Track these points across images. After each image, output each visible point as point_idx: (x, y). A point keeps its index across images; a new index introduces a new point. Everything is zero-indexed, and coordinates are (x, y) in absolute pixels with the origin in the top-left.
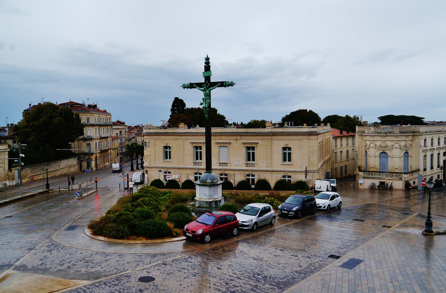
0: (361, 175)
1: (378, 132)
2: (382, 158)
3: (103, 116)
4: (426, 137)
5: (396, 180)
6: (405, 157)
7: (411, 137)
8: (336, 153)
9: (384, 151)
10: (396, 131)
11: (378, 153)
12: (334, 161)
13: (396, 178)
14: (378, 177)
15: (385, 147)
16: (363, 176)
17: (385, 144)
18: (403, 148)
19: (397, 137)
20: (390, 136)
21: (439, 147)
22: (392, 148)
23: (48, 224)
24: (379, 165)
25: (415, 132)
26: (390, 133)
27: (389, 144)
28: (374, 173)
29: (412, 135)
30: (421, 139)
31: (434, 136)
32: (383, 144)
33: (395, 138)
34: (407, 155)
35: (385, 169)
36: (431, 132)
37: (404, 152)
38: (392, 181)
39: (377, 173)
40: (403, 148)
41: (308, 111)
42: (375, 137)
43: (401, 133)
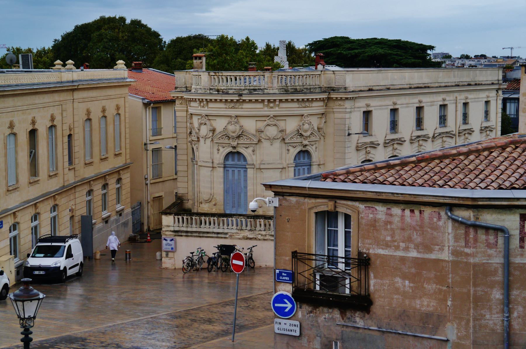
0: (168, 226)
1: (218, 91)
2: (230, 170)
4: (420, 102)
5: (264, 240)
6: (301, 168)
7: (321, 104)
8: (157, 152)
9: (234, 148)
10: (270, 85)
11: (219, 158)
12: (150, 176)
13: (263, 233)
14: (216, 230)
15: (239, 137)
16: (172, 229)
17: (238, 127)
18: (292, 138)
19: (272, 105)
20: (250, 101)
21: (419, 133)
22: (259, 141)
23: (114, 310)
24: (222, 193)
25: (333, 89)
26: (252, 91)
27: (250, 125)
28: (203, 218)
29: (323, 100)
30: (350, 112)
31: (399, 102)
32: (231, 128)
33: (266, 109)
34: (306, 160)
35: (239, 206)
36: (458, 86)
37: (294, 151)
38: (254, 243)
39: (212, 219)
40: (292, 138)
41: (128, 21)
42: (211, 105)
43: (286, 91)
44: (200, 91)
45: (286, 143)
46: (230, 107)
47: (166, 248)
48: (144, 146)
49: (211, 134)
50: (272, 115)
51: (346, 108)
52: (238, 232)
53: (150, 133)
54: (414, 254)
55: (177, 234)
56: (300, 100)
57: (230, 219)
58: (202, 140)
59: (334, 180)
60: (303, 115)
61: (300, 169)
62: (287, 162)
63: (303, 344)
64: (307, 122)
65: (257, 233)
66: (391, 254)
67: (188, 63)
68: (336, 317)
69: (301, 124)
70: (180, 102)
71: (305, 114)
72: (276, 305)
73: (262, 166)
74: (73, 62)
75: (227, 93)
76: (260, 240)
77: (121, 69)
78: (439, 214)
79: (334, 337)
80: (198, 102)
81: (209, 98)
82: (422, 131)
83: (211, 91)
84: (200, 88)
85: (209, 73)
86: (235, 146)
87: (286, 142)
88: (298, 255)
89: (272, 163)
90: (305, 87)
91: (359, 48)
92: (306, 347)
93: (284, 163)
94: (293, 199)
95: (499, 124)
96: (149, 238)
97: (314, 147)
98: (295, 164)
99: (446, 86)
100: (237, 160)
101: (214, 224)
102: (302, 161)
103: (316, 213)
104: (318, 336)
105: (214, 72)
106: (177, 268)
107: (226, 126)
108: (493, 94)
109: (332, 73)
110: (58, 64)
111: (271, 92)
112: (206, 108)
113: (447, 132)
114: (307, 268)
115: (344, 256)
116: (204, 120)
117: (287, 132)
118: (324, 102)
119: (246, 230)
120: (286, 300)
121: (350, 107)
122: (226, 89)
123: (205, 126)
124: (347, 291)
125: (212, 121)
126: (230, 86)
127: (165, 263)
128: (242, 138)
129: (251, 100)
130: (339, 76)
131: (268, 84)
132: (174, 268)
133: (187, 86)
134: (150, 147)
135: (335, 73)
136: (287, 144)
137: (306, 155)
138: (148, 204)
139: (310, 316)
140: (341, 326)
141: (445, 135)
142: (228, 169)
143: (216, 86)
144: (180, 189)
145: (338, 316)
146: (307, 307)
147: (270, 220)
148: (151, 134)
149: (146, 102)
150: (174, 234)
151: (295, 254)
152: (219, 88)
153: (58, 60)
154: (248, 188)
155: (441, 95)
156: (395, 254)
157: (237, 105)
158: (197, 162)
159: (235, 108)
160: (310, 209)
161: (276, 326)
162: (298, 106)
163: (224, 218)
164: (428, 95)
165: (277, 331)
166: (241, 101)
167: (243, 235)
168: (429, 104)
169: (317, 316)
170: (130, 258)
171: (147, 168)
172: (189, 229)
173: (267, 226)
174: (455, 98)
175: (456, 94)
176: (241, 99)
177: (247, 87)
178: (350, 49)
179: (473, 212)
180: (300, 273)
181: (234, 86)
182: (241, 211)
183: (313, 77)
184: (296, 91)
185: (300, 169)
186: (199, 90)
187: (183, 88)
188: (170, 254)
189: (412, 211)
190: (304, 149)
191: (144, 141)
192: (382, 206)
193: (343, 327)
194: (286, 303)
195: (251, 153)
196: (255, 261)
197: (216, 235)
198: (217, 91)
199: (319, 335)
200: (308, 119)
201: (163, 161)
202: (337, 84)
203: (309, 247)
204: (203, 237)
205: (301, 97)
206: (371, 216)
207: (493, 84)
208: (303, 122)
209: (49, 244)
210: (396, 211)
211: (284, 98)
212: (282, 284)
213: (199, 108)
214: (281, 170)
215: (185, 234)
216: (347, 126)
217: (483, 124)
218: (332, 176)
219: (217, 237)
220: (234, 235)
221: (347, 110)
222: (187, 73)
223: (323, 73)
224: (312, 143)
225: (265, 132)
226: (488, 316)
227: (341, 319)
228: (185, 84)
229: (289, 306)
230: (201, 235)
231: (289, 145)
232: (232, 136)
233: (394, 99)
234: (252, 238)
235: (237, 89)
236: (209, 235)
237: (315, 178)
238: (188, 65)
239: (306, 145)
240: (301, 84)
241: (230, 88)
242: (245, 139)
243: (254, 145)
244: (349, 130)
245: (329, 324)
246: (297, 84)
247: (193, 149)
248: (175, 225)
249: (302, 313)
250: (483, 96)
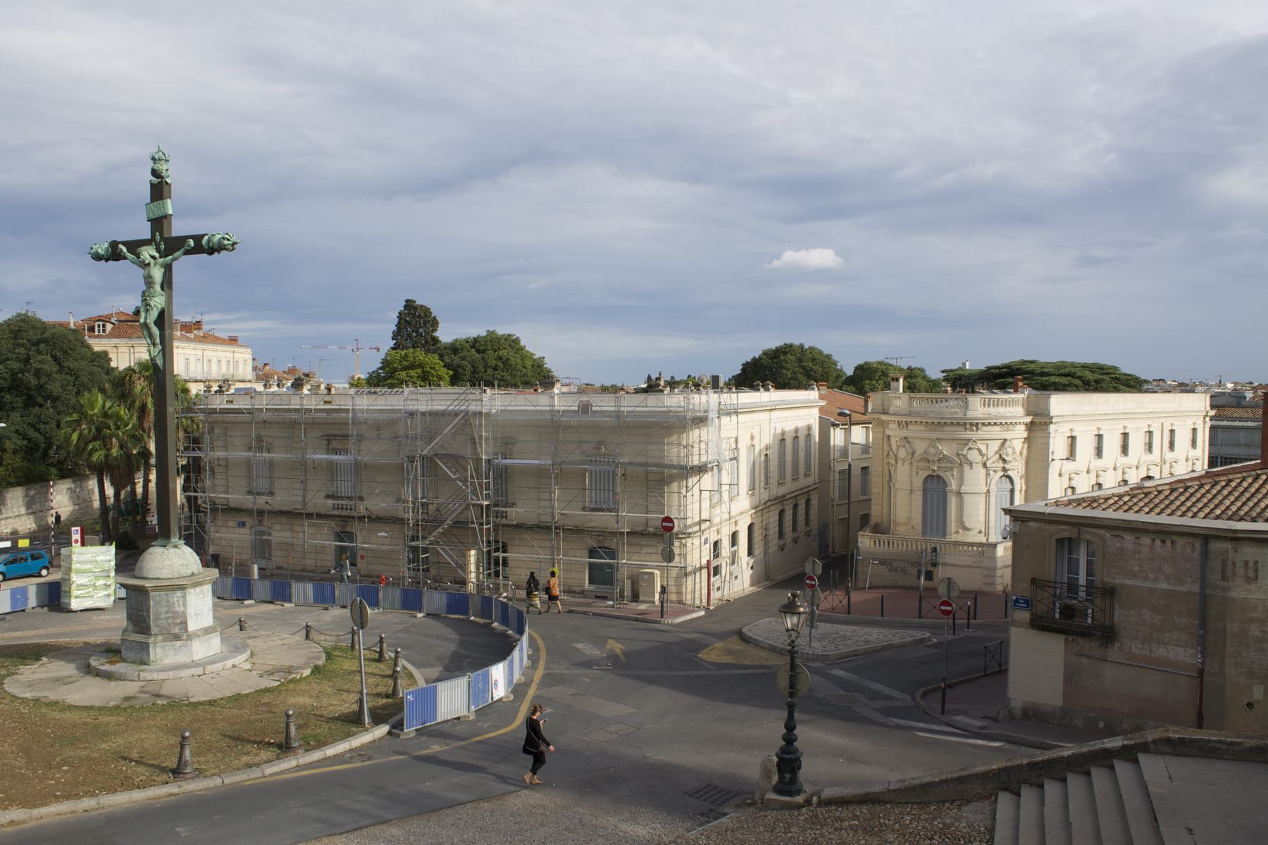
3: (219, 354)
54: (1164, 586)
58: (900, 463)
66: (1139, 584)
78: (1193, 545)
81: (908, 420)
94: (1033, 525)
99: (1151, 412)
103: (1057, 540)
114: (1046, 595)
115: (1085, 584)
124: (1089, 621)
156: (1143, 585)
162: (1000, 430)
179: (1231, 544)
180: (1039, 601)
189: (1163, 541)
192: (1130, 535)
206: (1118, 545)
210: (1146, 540)
226: (1244, 654)
247: (890, 471)
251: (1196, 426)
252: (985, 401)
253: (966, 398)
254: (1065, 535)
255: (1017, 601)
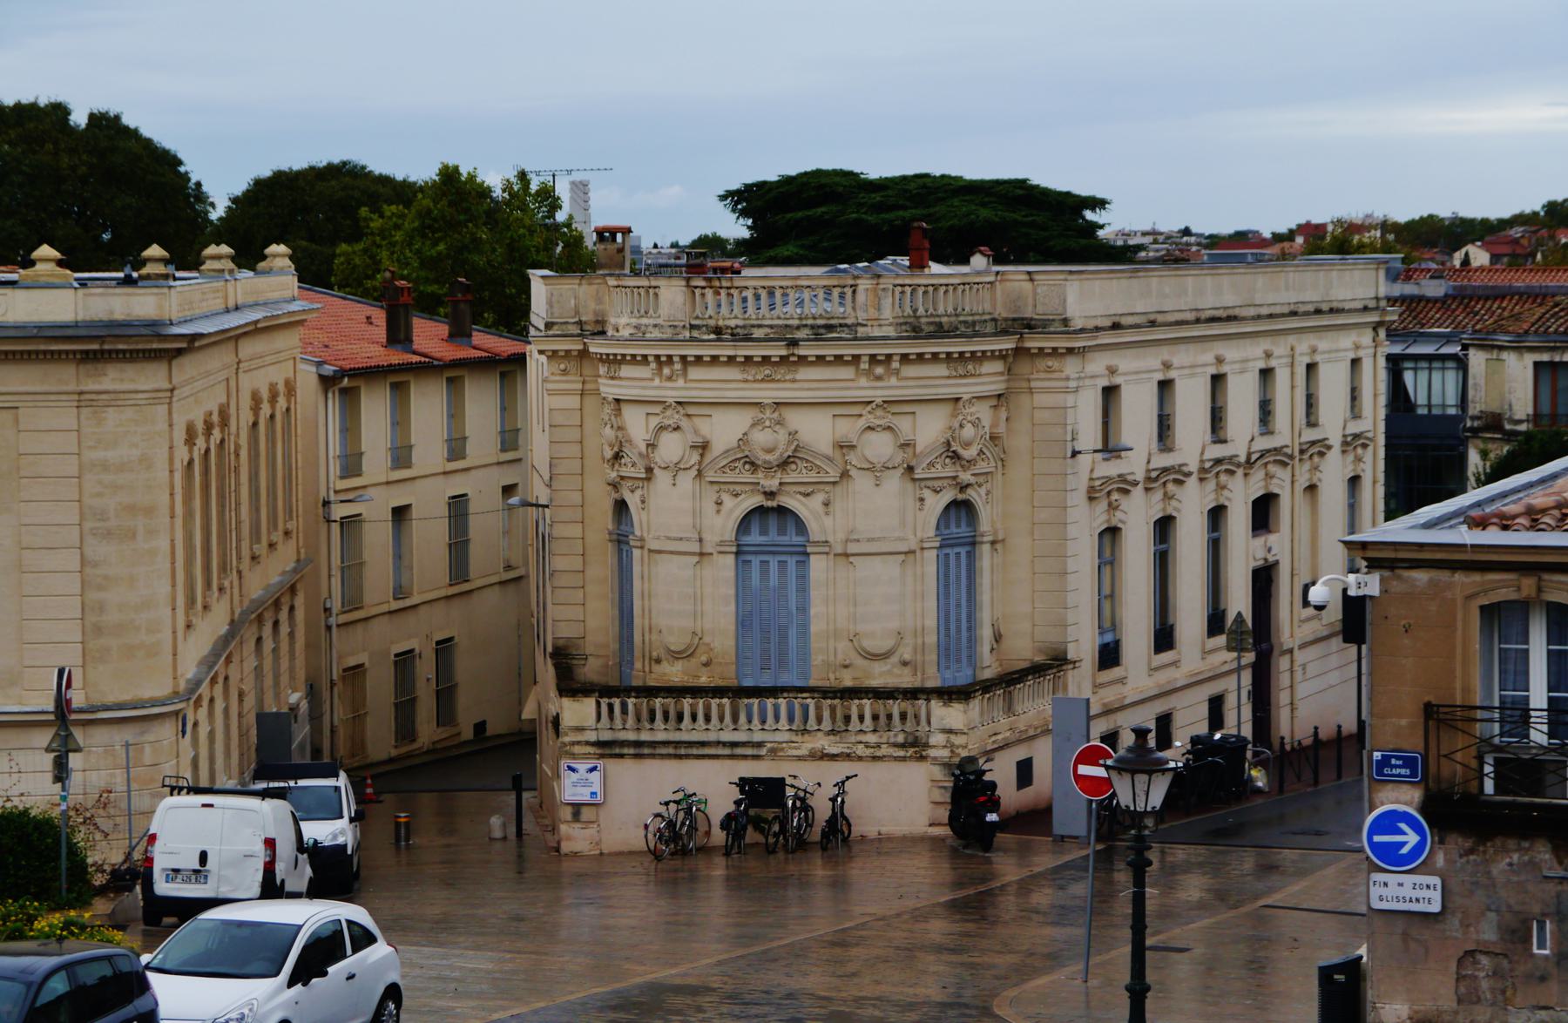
0: (580, 729)
1: (718, 331)
2: (756, 561)
5: (875, 758)
7: (998, 366)
8: (350, 524)
9: (770, 495)
10: (872, 313)
11: (722, 523)
12: (336, 605)
13: (872, 738)
14: (727, 736)
15: (784, 464)
16: (592, 736)
17: (782, 436)
18: (931, 464)
19: (879, 370)
20: (821, 360)
22: (845, 475)
24: (732, 628)
25: (1029, 325)
26: (823, 330)
27: (818, 431)
28: (687, 703)
29: (1002, 356)
30: (1077, 390)
32: (761, 438)
33: (863, 382)
34: (963, 530)
35: (783, 663)
37: (937, 503)
38: (841, 769)
39: (714, 702)
40: (931, 464)
42: (695, 373)
43: (915, 331)
44: (656, 334)
45: (914, 480)
46: (759, 377)
47: (574, 795)
48: (321, 510)
49: (695, 458)
50: (879, 400)
51: (1068, 379)
52: (794, 738)
53: (335, 468)
55: (608, 751)
56: (927, 356)
57: (770, 702)
59: (1505, 528)
60: (958, 400)
61: (959, 553)
62: (919, 535)
63: (1448, 933)
64: (969, 418)
65: (853, 739)
67: (338, 251)
68: (1541, 860)
69: (957, 425)
70: (562, 367)
71: (966, 397)
72: (1377, 839)
73: (852, 548)
74: (55, 254)
75: (748, 338)
76: (860, 758)
77: (282, 271)
79: (1536, 909)
80: (653, 365)
81: (692, 351)
82: (1224, 445)
83: (695, 334)
84: (655, 326)
85: (688, 280)
86: (774, 489)
87: (917, 476)
88: (1441, 709)
89: (878, 539)
90: (962, 318)
91: (908, 204)
92: (1456, 938)
93: (912, 537)
94: (1421, 577)
95: (1382, 427)
96: (369, 790)
97: (983, 491)
98: (939, 539)
99: (1271, 316)
100: (758, 532)
101: (721, 719)
102: (955, 530)
103: (1482, 608)
104: (1490, 910)
105: (705, 279)
106: (605, 851)
107: (745, 434)
108: (1366, 338)
109: (1026, 277)
110: (218, 257)
111: (877, 333)
112: (681, 382)
113: (1275, 449)
116: (672, 418)
117: (919, 449)
118: (1005, 362)
119: (820, 734)
120: (1403, 826)
121: (1077, 375)
122: (744, 327)
123: (676, 435)
125: (696, 420)
126: (754, 317)
127: (569, 838)
128: (793, 467)
129: (823, 357)
130: (1045, 288)
131: (866, 311)
132: (598, 852)
133: (583, 319)
134: (339, 511)
135: (1036, 277)
136: (917, 484)
137: (963, 513)
138: (332, 688)
139: (1468, 862)
140: (1557, 881)
141: (1271, 459)
142: (748, 557)
143: (710, 317)
144: (563, 624)
145: (1547, 856)
146: (1460, 840)
147: (891, 701)
148: (338, 473)
149: (332, 373)
150: (599, 751)
151: (1429, 710)
152: (721, 323)
153: (155, 246)
154: (813, 612)
155: (1261, 340)
157: (781, 373)
158: (642, 539)
159: (773, 381)
160: (1469, 597)
161: (1375, 892)
163: (751, 701)
164: (1234, 342)
165: (1376, 905)
166: (792, 359)
167: (810, 746)
168: (1186, 371)
169: (1487, 860)
170: (407, 840)
171: (330, 576)
172: (645, 736)
173: (883, 719)
174: (1289, 349)
175: (1292, 339)
176: (793, 355)
177: (806, 318)
178: (880, 208)
180: (1445, 756)
181: (768, 316)
182: (789, 679)
183: (964, 291)
184: (941, 331)
185: (959, 553)
186: (650, 329)
187: (570, 327)
188: (584, 810)
190: (961, 497)
191: (323, 493)
193: (1561, 883)
194: (1404, 833)
195: (820, 509)
196: (851, 821)
197: (727, 751)
198: (714, 333)
199: (1493, 907)
200: (973, 409)
201: (366, 556)
202: (1040, 309)
203: (1466, 690)
204: (687, 756)
205: (955, 347)
207: (1366, 309)
208: (961, 417)
209: (272, 785)
211: (913, 349)
212: (1390, 786)
213: (657, 382)
214: (902, 557)
215: (632, 751)
216: (1069, 428)
217: (1349, 425)
218: (1494, 520)
219: (732, 757)
220: (782, 749)
221: (1072, 384)
222: (583, 282)
223: (999, 278)
224: (981, 479)
225: (859, 448)
227: (1556, 865)
228: (577, 313)
229: (1412, 838)
230: (683, 751)
231: (923, 484)
232: (765, 462)
233: (1165, 353)
234: (837, 755)
235: (777, 326)
236: (707, 751)
237: (1436, 524)
238: (342, 259)
239: (968, 486)
240: (950, 310)
241: (755, 322)
242: (804, 471)
243: (827, 488)
244: (1073, 439)
245: (1523, 877)
246: (941, 310)
248: (599, 726)
249: (1445, 855)
250: (1346, 341)
251: (1273, 363)
252: (903, 292)
253: (1476, 270)
254: (1506, 594)
255: (1385, 761)
